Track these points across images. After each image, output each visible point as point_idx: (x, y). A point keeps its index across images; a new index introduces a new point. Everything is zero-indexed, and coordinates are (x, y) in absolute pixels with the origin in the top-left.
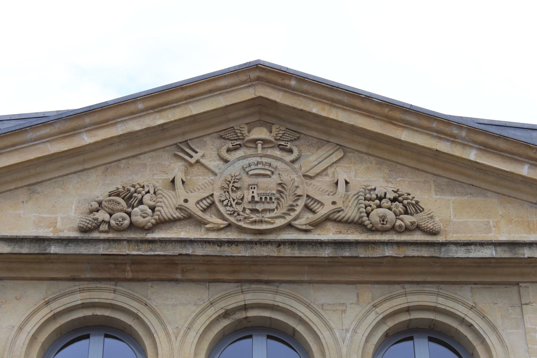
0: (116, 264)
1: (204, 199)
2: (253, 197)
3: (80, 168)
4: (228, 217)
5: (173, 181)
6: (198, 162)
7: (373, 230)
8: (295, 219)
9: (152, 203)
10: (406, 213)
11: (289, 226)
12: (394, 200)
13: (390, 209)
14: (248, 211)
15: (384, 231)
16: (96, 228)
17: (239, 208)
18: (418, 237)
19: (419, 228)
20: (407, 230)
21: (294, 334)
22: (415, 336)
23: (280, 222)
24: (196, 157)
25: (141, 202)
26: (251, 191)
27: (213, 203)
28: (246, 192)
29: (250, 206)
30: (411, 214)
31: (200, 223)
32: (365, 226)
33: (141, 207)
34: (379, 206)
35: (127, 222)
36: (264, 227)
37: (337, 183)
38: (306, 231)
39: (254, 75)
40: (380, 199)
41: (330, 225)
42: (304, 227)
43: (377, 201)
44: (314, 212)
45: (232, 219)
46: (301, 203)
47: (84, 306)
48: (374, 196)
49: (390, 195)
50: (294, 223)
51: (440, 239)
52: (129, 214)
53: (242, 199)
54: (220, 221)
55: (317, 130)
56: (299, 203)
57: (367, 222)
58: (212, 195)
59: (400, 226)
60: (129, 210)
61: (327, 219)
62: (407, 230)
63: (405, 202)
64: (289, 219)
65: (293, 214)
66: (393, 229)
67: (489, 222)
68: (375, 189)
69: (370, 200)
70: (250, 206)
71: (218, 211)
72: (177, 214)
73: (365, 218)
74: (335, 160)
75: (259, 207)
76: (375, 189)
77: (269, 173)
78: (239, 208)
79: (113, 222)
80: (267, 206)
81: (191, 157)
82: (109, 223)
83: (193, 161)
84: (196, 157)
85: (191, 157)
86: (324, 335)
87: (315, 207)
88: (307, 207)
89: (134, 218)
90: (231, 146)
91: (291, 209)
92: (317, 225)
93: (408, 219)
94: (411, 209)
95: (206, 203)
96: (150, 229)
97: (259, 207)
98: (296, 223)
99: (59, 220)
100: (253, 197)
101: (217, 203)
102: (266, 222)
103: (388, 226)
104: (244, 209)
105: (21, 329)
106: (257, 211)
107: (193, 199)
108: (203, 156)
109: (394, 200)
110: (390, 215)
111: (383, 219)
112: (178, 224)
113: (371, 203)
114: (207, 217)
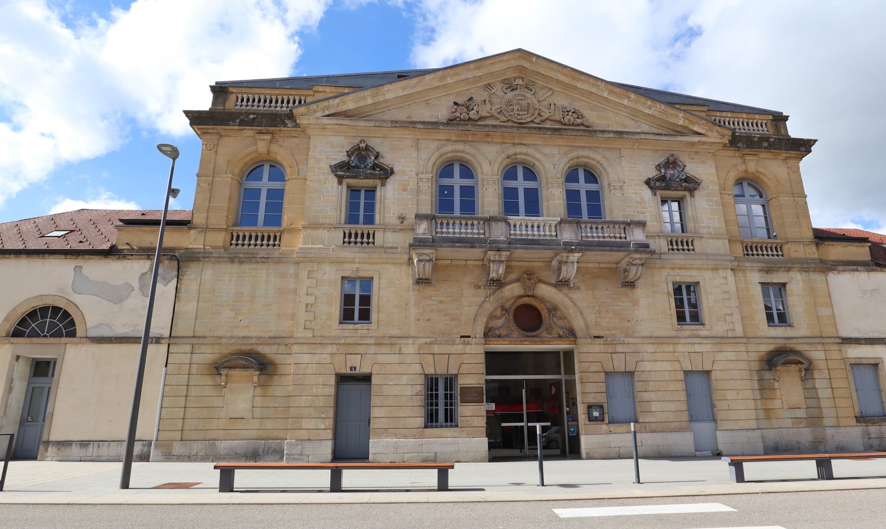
0: (465, 135)
1: (498, 109)
2: (518, 109)
3: (445, 93)
4: (507, 116)
5: (485, 101)
6: (494, 93)
7: (565, 125)
8: (535, 119)
9: (477, 110)
10: (578, 118)
11: (532, 121)
12: (573, 113)
13: (572, 116)
14: (516, 115)
15: (569, 125)
16: (455, 119)
17: (512, 113)
18: (582, 128)
19: (583, 125)
20: (578, 125)
21: (534, 165)
22: (265, 164)
23: (529, 120)
24: (493, 91)
25: (473, 109)
26: (517, 106)
27: (501, 111)
28: (515, 106)
29: (517, 112)
30: (580, 119)
31: (497, 119)
32: (562, 123)
33: (473, 111)
34: (568, 115)
35: (468, 117)
36: (522, 121)
37: (550, 105)
38: (539, 124)
39: (518, 55)
40: (568, 112)
41: (548, 122)
42: (538, 122)
43: (567, 113)
44: (541, 116)
45: (510, 118)
46: (537, 112)
47: (452, 151)
48: (566, 111)
49: (573, 110)
50: (534, 120)
51: (590, 129)
52: (468, 114)
53: (513, 109)
54: (505, 118)
55: (541, 81)
56: (536, 112)
57: (563, 121)
58: (501, 107)
59: (576, 124)
60: (468, 112)
61: (547, 119)
62: (578, 125)
63: (578, 113)
64: (532, 118)
65: (534, 116)
66: (573, 124)
67: (609, 124)
68: (566, 108)
69: (564, 112)
70: (517, 112)
71: (504, 114)
72: (488, 115)
73: (562, 120)
74: (549, 94)
75: (520, 113)
76: (566, 108)
77: (524, 99)
78: (512, 113)
79: (462, 117)
80: (524, 113)
81: (491, 91)
82: (460, 117)
83: (492, 92)
84: (493, 91)
85: (491, 91)
86: (609, 170)
87: (542, 114)
88: (539, 114)
89: (471, 116)
90: (507, 86)
91: (533, 115)
92: (543, 121)
93: (579, 121)
94: (580, 117)
95: (498, 111)
96: (477, 121)
97: (520, 113)
98: (535, 121)
99: (440, 116)
100: (518, 109)
101: (503, 111)
102: (523, 119)
103: (571, 123)
104: (514, 114)
105: (429, 160)
106: (519, 115)
107: (494, 108)
108: (496, 91)
109: (573, 113)
110: (572, 119)
111: (569, 120)
112: (488, 118)
113: (565, 113)
114: (499, 116)
